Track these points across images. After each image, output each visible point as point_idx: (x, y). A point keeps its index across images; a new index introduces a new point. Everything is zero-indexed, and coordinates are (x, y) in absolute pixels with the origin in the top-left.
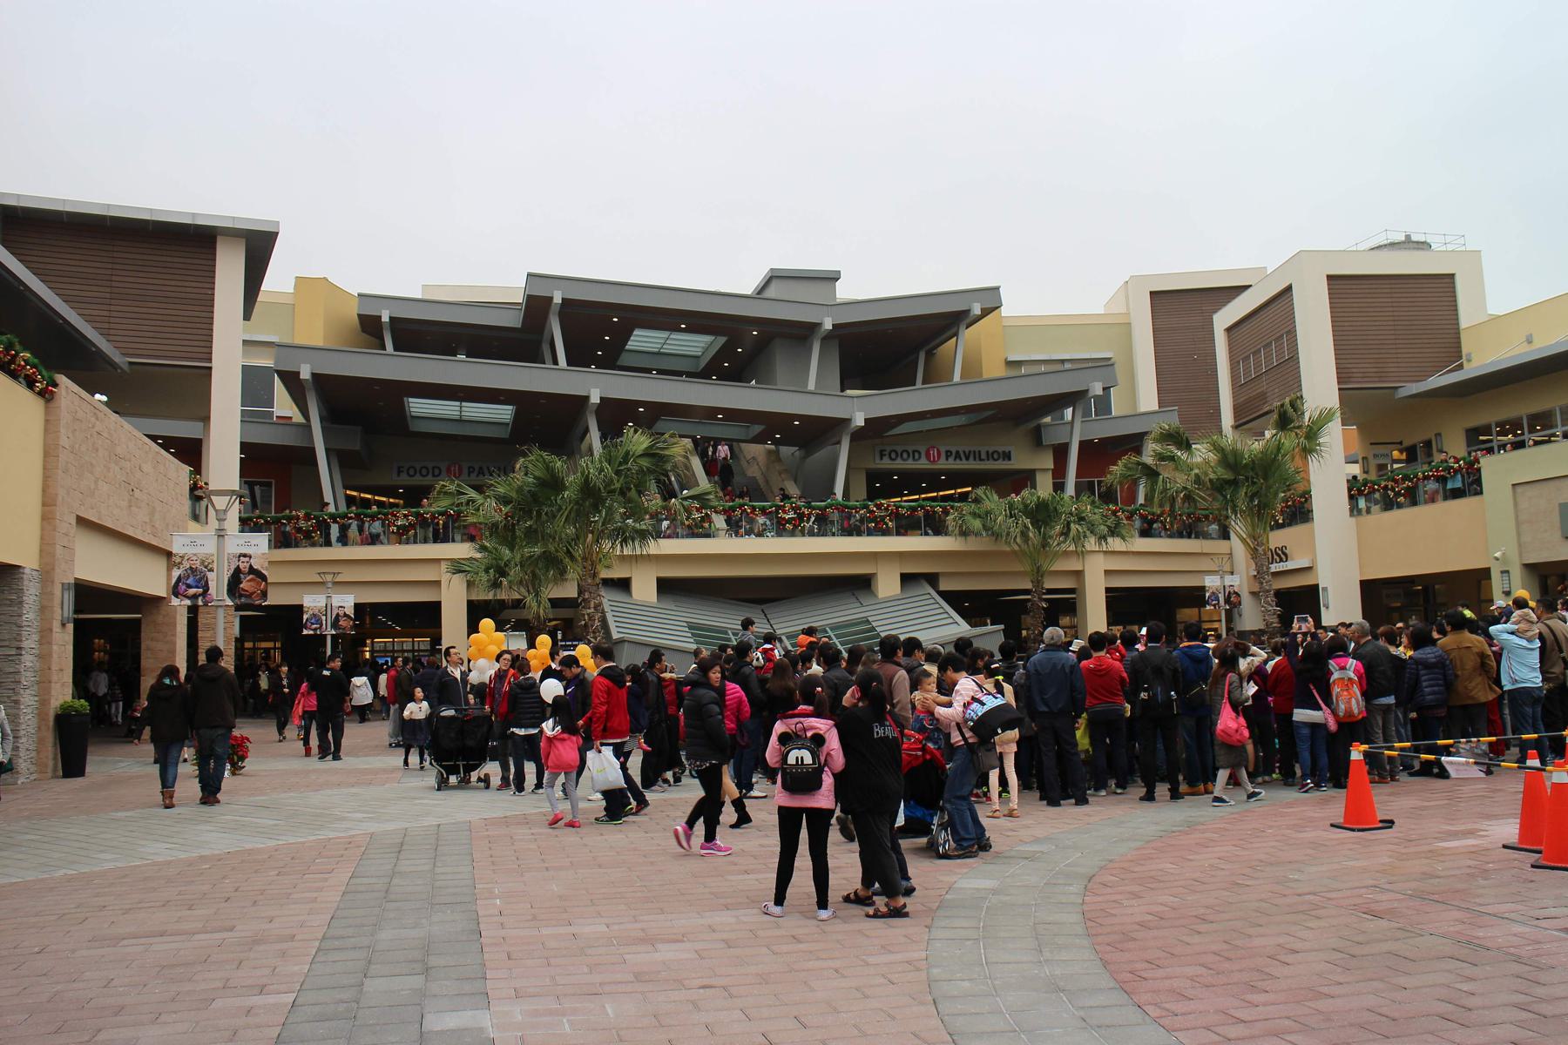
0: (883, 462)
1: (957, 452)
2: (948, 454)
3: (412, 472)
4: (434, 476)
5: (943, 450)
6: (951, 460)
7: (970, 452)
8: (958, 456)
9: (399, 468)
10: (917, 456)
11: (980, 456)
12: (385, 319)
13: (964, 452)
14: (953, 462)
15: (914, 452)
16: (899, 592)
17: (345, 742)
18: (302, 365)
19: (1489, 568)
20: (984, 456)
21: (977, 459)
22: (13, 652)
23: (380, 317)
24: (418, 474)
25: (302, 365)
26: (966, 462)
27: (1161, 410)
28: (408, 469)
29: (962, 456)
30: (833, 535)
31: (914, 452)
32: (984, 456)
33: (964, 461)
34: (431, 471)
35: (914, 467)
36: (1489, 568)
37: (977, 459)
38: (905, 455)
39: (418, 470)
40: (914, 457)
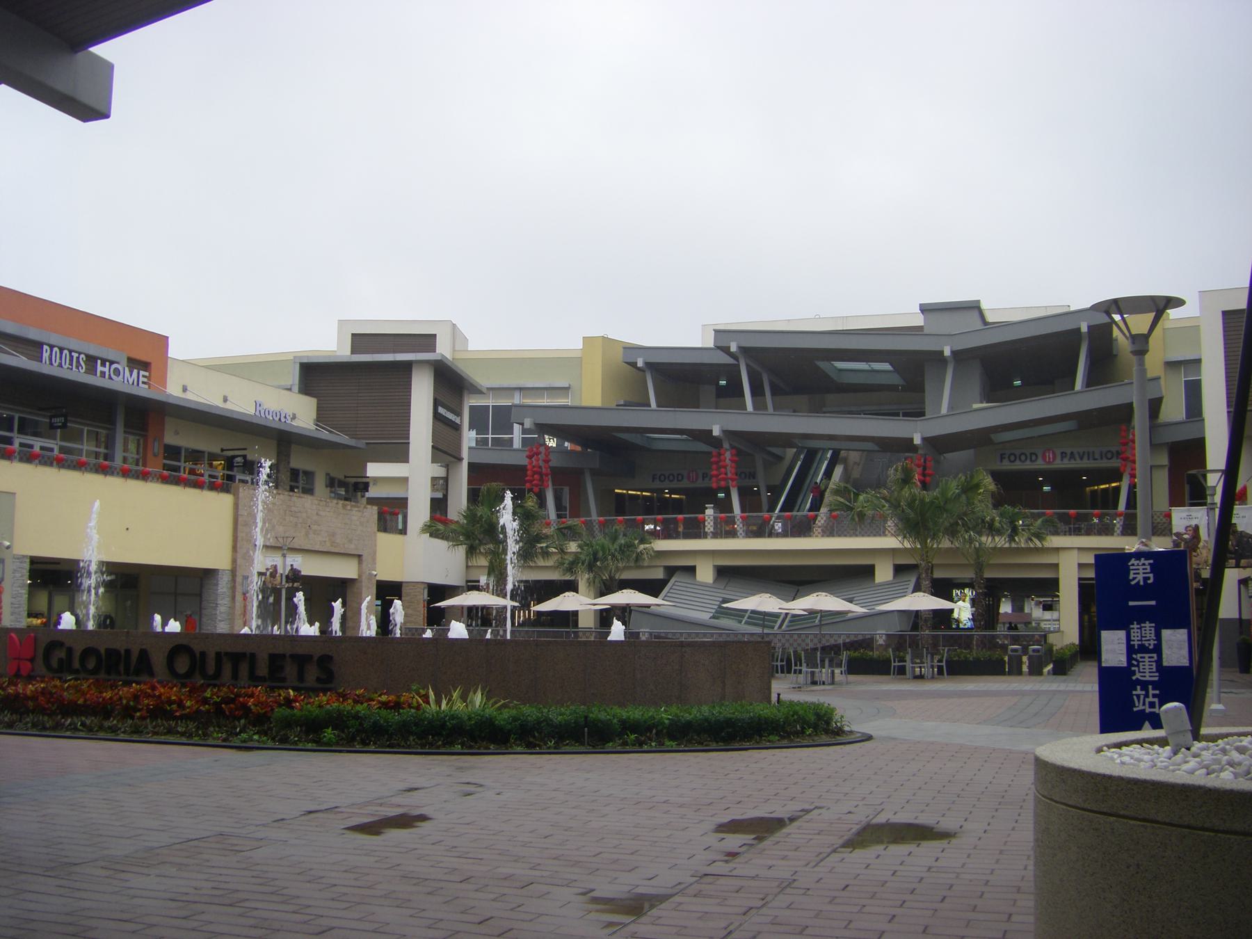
0: (1004, 464)
1: (1072, 453)
2: (1063, 455)
3: (662, 478)
4: (678, 480)
5: (1058, 452)
6: (1066, 461)
7: (1084, 452)
8: (1072, 456)
9: (1002, 455)
10: (1034, 458)
11: (1093, 455)
12: (947, 352)
13: (1079, 453)
14: (1068, 462)
15: (1031, 454)
16: (711, 582)
17: (441, 544)
18: (945, 347)
19: (407, 461)
20: (1097, 456)
21: (1091, 458)
22: (214, 605)
23: (712, 431)
24: (667, 476)
25: (945, 347)
26: (1088, 462)
27: (1188, 420)
28: (660, 477)
29: (1077, 456)
30: (816, 536)
31: (1031, 454)
32: (1097, 456)
33: (1078, 461)
34: (1029, 457)
35: (1009, 468)
36: (407, 461)
37: (1091, 458)
38: (671, 478)
39: (1018, 456)
40: (1031, 458)
